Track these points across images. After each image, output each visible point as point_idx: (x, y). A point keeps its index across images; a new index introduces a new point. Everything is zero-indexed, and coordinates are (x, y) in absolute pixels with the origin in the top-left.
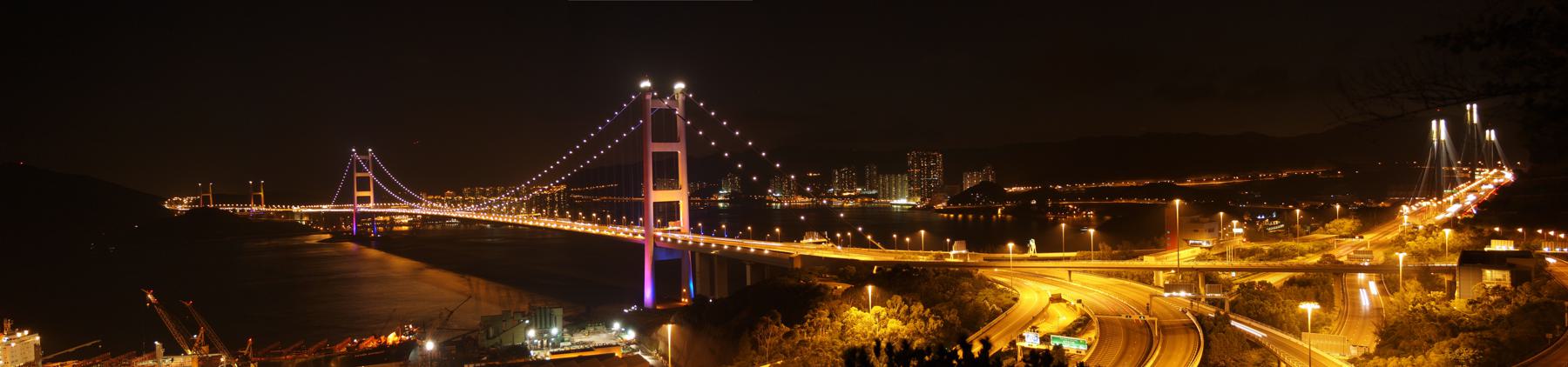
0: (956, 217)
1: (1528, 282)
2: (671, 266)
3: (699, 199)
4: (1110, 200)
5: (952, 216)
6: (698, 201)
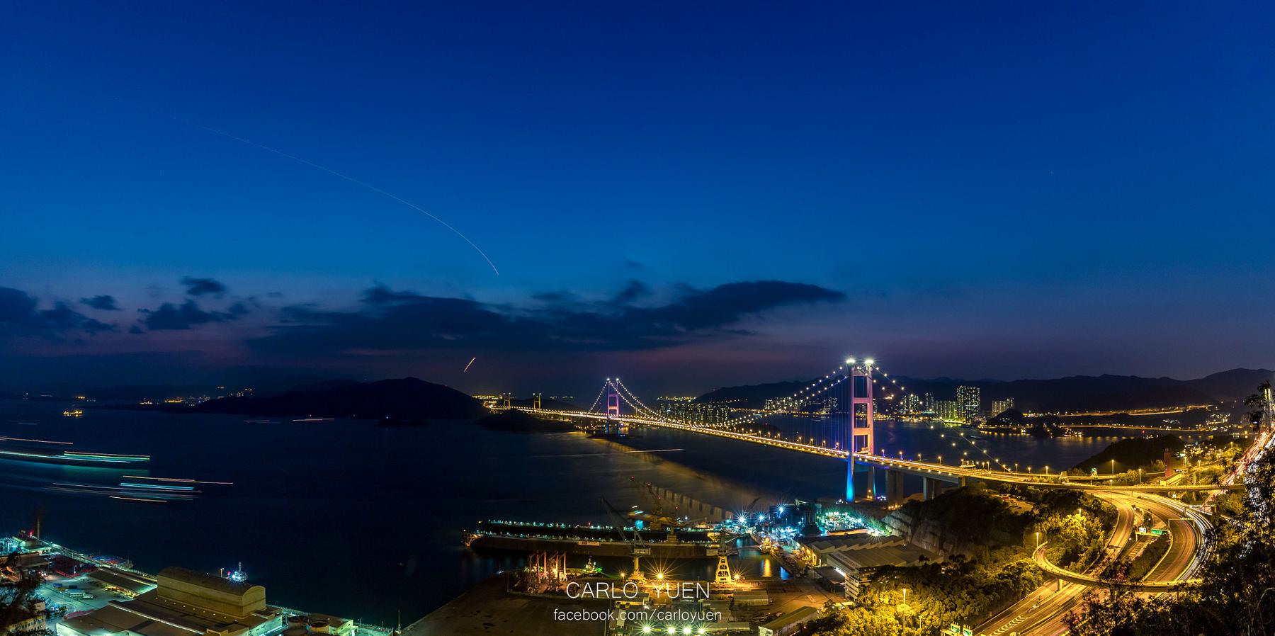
0: (993, 434)
1: (911, 591)
2: (865, 475)
3: (808, 413)
4: (1092, 424)
5: (990, 433)
6: (807, 415)
